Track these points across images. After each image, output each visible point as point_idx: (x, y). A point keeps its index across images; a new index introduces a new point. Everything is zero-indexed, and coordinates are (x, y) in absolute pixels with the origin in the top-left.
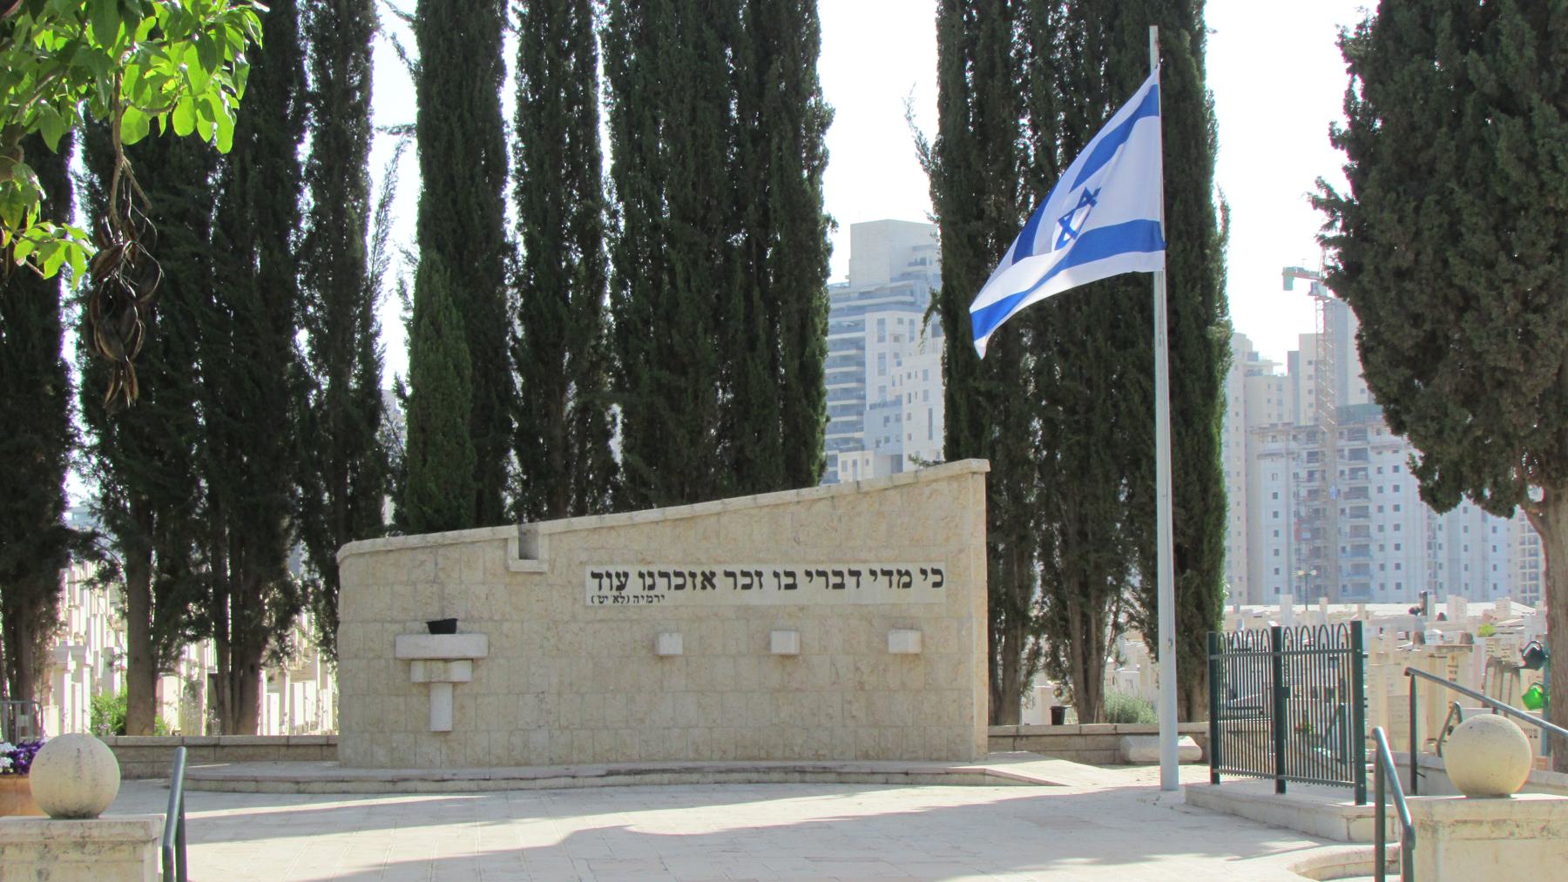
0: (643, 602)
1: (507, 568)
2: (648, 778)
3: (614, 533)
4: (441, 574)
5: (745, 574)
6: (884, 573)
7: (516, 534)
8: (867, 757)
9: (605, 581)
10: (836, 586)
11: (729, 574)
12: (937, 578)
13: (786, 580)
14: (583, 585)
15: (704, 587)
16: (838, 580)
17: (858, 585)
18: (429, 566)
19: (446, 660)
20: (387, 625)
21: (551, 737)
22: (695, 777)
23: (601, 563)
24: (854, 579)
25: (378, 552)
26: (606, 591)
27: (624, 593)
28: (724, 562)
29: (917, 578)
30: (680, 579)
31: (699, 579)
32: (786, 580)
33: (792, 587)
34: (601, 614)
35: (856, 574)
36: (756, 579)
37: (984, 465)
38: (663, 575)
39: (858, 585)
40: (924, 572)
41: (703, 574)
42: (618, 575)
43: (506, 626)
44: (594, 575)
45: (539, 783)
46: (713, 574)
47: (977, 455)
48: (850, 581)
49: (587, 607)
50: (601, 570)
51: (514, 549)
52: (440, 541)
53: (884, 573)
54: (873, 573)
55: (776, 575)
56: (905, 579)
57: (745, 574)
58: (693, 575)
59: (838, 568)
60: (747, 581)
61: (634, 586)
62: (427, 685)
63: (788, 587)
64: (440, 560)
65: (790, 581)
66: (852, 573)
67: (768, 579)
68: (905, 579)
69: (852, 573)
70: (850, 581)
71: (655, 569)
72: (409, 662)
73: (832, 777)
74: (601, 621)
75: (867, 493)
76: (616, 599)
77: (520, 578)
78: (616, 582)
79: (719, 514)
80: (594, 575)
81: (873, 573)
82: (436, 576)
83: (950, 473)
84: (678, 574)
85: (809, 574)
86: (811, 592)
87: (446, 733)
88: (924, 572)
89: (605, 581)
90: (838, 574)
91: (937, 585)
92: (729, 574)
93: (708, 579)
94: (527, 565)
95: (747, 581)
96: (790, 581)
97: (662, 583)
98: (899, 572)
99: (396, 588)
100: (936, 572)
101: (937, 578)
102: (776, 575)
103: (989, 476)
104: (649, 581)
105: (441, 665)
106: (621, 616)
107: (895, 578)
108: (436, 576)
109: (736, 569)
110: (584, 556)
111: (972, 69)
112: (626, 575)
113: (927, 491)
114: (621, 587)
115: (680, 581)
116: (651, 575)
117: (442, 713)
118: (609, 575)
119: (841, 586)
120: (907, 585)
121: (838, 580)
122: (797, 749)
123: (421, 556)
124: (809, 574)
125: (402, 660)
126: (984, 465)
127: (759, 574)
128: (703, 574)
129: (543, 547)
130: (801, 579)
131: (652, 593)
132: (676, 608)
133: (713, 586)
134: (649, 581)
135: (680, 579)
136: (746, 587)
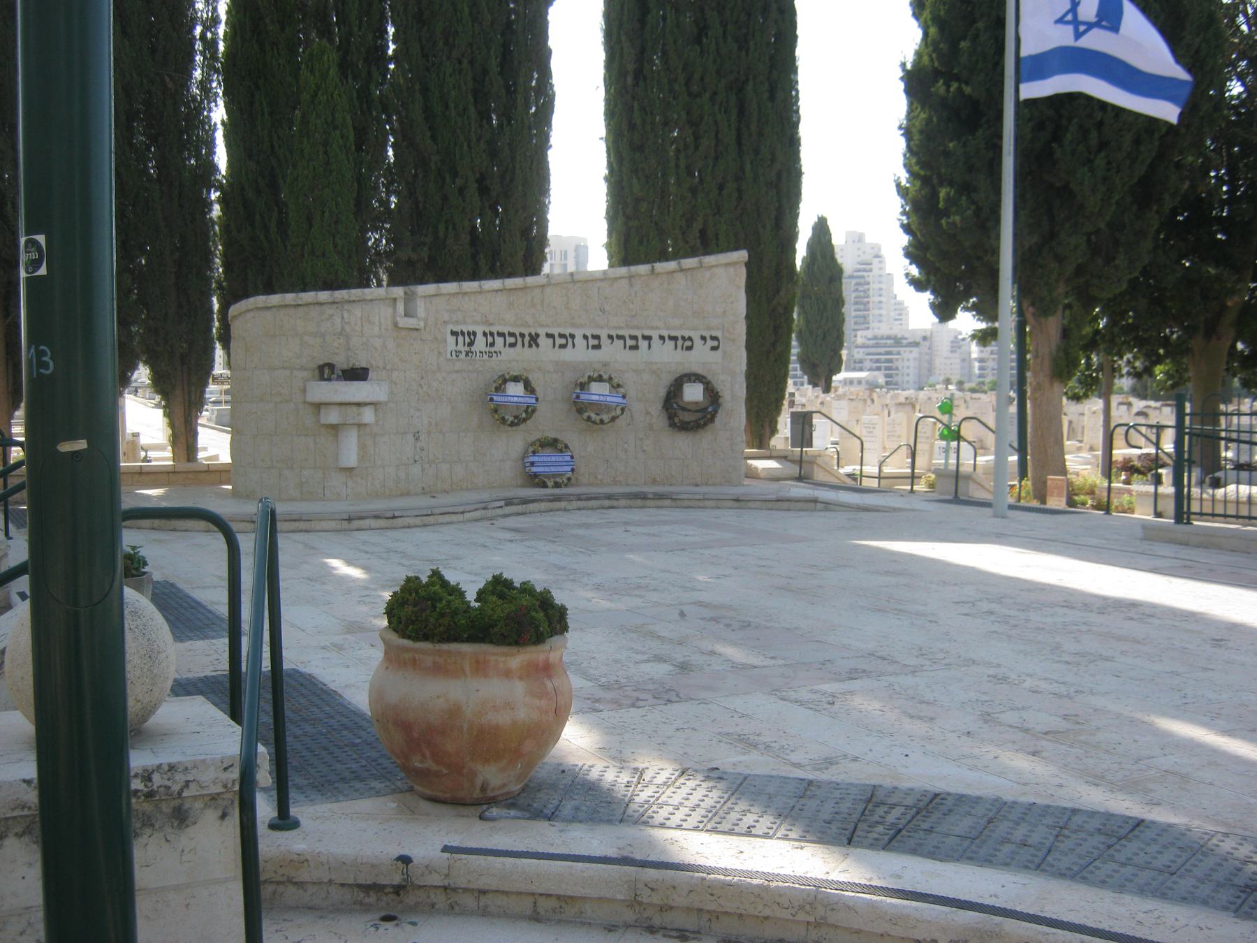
0: (485, 357)
1: (396, 325)
2: (531, 507)
3: (466, 298)
4: (348, 329)
5: (561, 336)
6: (671, 338)
7: (402, 294)
8: (654, 482)
9: (461, 339)
10: (632, 348)
11: (549, 336)
12: (715, 343)
13: (592, 342)
14: (445, 341)
15: (530, 346)
16: (633, 343)
17: (650, 347)
18: (338, 320)
19: (359, 405)
20: (296, 373)
21: (423, 470)
22: (563, 504)
23: (457, 322)
24: (646, 343)
25: (286, 306)
26: (460, 347)
27: (473, 349)
28: (547, 326)
29: (698, 342)
30: (513, 339)
31: (527, 339)
32: (592, 342)
33: (598, 347)
34: (458, 366)
35: (649, 338)
36: (519, 340)
37: (743, 255)
38: (501, 334)
39: (650, 347)
40: (703, 338)
41: (530, 335)
42: (469, 333)
43: (395, 374)
44: (454, 333)
45: (468, 516)
46: (537, 335)
47: (736, 249)
48: (643, 344)
49: (448, 360)
50: (457, 329)
51: (401, 307)
52: (346, 297)
53: (671, 338)
54: (662, 338)
55: (585, 337)
56: (688, 343)
57: (561, 336)
58: (522, 335)
59: (634, 333)
60: (563, 341)
61: (480, 343)
62: (335, 428)
63: (594, 347)
64: (346, 315)
65: (596, 342)
66: (645, 337)
67: (579, 340)
68: (688, 343)
69: (645, 337)
70: (643, 344)
71: (495, 329)
72: (318, 406)
73: (667, 502)
74: (457, 372)
75: (659, 274)
76: (467, 354)
77: (404, 333)
78: (467, 340)
79: (543, 286)
80: (454, 333)
81: (662, 338)
82: (343, 329)
83: (728, 260)
84: (511, 335)
85: (610, 337)
86: (612, 353)
87: (352, 469)
88: (703, 338)
89: (461, 339)
90: (634, 338)
91: (714, 348)
92: (549, 336)
93: (534, 339)
94: (411, 322)
95: (563, 341)
96: (596, 342)
97: (499, 341)
98: (683, 338)
99: (306, 338)
100: (714, 338)
101: (715, 343)
102: (585, 337)
103: (748, 265)
104: (490, 339)
105: (354, 408)
106: (471, 368)
107: (680, 343)
108: (343, 329)
109: (555, 331)
110: (446, 318)
111: (219, 200)
112: (475, 334)
113: (708, 274)
114: (471, 344)
115: (512, 340)
116: (492, 334)
117: (350, 452)
118: (463, 333)
119: (636, 347)
120: (690, 348)
121: (633, 343)
122: (599, 477)
123: (329, 311)
124: (610, 337)
125: (312, 404)
126: (743, 255)
127: (573, 336)
128: (530, 335)
129: (421, 308)
130: (605, 341)
131: (492, 349)
132: (510, 362)
133: (537, 345)
134: (490, 339)
135: (513, 339)
136: (562, 346)
